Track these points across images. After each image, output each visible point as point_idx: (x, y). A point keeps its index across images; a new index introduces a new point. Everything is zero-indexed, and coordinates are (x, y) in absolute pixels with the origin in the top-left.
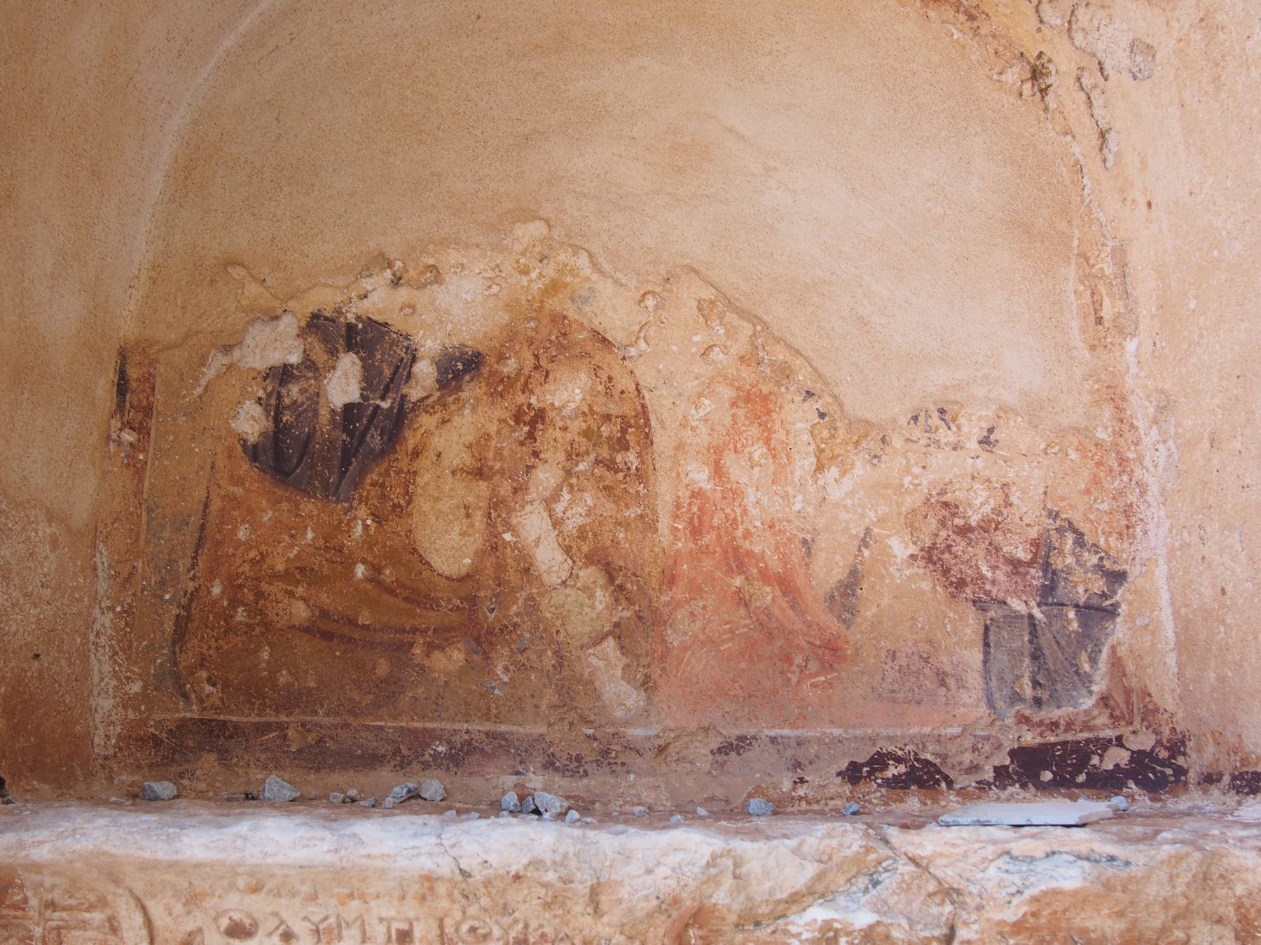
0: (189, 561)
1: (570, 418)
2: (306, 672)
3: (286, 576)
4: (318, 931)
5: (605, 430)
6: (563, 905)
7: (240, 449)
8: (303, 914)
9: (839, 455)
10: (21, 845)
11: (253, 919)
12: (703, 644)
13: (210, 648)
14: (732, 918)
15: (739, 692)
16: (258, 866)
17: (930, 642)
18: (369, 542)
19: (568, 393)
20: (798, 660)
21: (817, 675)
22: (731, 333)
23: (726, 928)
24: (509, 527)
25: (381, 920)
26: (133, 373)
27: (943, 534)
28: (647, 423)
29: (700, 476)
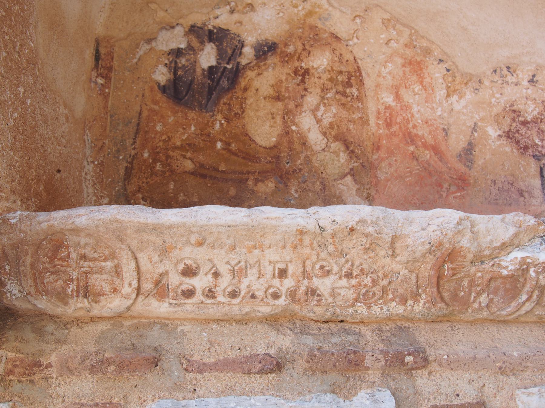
0: (131, 141)
1: (322, 73)
2: (193, 194)
3: (181, 148)
4: (233, 271)
5: (340, 78)
6: (374, 250)
7: (156, 87)
8: (226, 260)
9: (457, 90)
10: (69, 217)
11: (198, 264)
12: (396, 178)
13: (143, 183)
14: (470, 256)
15: (417, 201)
16: (204, 226)
17: (513, 175)
18: (223, 131)
19: (320, 61)
20: (446, 185)
21: (456, 192)
22: (400, 33)
23: (466, 264)
24: (294, 123)
25: (270, 262)
26: (103, 51)
27: (514, 125)
29: (389, 99)
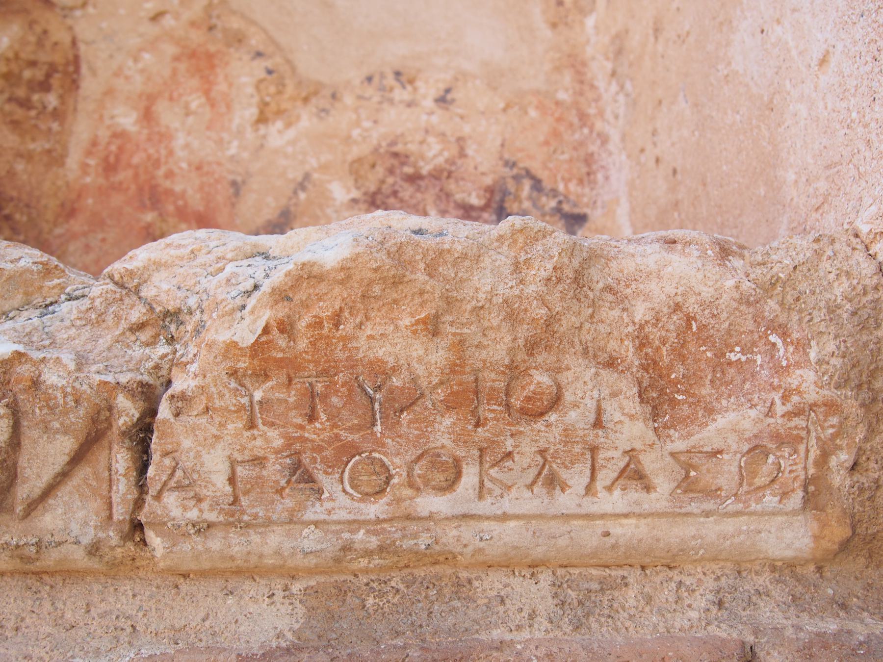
28: (77, 70)
